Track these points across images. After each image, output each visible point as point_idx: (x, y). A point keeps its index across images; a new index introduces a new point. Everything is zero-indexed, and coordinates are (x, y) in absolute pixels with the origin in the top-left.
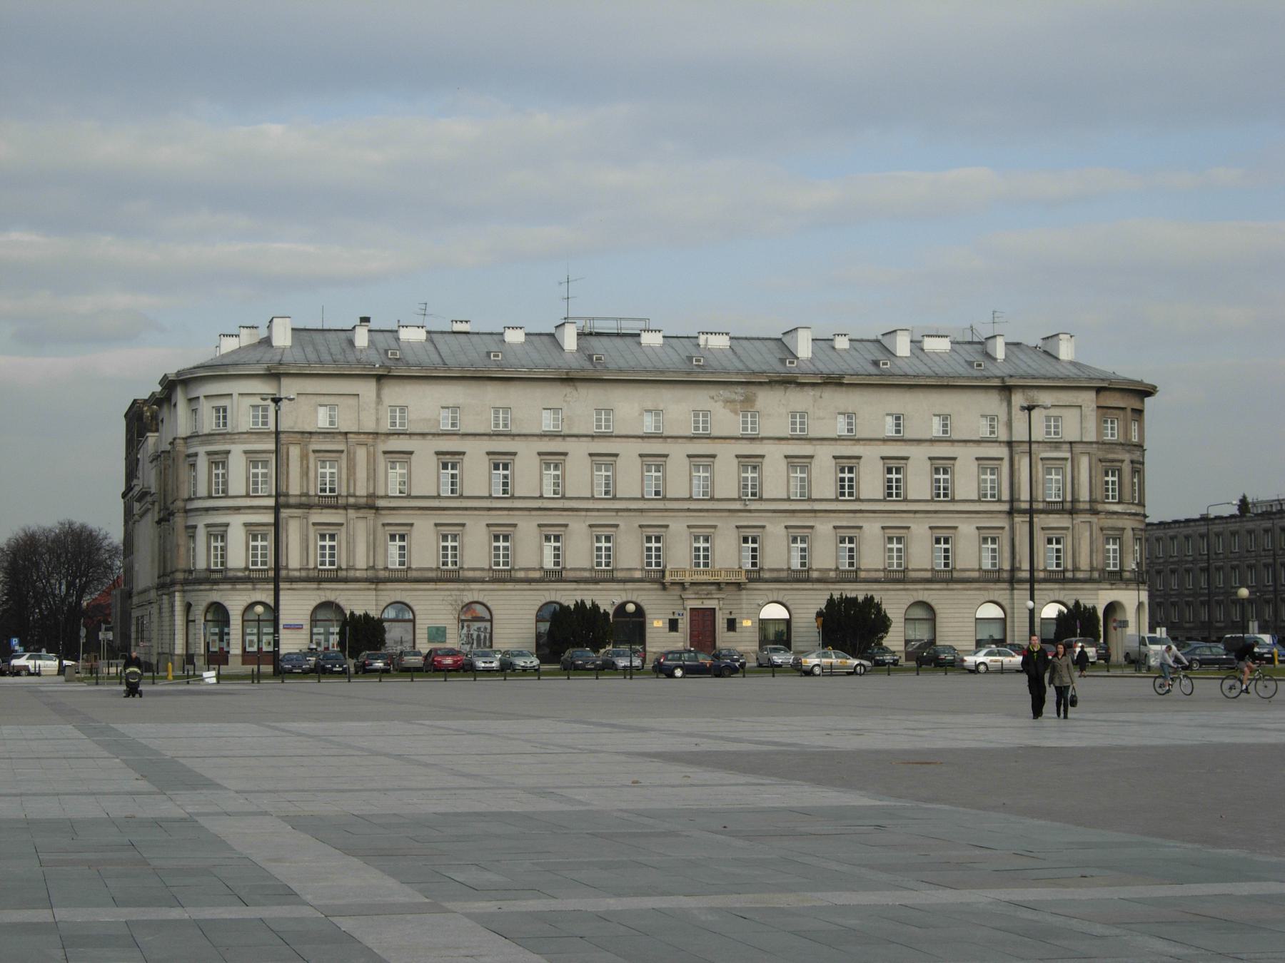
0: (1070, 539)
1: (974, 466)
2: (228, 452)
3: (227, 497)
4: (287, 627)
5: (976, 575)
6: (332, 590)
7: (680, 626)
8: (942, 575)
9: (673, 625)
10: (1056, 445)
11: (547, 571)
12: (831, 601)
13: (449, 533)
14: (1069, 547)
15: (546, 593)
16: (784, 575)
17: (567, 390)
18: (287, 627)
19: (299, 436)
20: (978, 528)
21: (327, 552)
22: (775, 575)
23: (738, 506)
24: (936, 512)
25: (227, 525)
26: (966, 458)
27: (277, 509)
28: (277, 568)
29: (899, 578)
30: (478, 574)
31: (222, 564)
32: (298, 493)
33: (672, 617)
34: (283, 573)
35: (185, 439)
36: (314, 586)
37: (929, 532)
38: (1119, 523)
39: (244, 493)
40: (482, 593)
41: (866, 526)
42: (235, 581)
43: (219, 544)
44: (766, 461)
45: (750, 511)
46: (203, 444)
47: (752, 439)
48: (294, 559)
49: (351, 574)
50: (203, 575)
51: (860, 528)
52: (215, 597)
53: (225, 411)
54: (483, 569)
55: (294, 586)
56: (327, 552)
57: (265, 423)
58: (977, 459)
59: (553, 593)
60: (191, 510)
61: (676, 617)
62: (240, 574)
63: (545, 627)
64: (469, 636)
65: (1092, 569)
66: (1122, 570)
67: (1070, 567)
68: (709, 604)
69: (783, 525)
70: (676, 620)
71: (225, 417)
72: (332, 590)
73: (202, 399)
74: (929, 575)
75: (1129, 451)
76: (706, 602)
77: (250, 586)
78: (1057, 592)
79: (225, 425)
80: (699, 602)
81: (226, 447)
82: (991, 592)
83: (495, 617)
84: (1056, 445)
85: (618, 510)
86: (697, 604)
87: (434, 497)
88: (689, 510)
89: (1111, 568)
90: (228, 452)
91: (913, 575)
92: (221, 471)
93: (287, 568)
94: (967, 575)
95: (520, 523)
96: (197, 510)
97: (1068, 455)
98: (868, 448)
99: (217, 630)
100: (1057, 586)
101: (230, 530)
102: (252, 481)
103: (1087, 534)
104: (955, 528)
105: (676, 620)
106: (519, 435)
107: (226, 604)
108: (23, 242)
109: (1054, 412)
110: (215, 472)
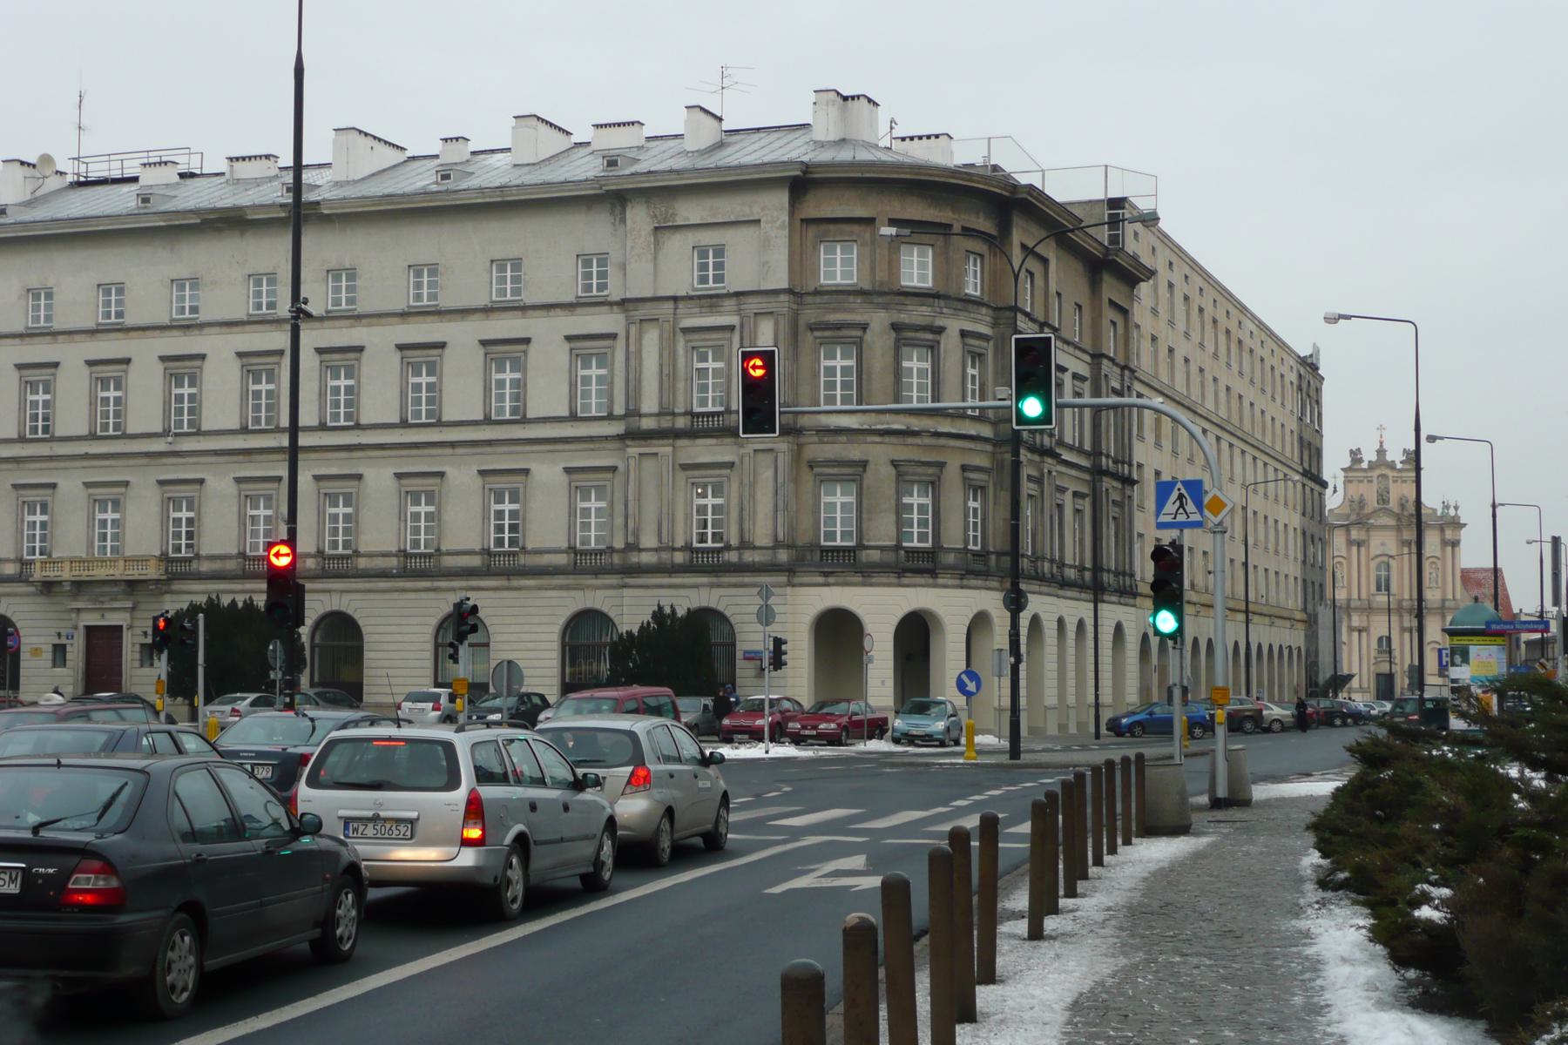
0: (735, 486)
1: (562, 353)
5: (562, 559)
7: (69, 656)
8: (502, 562)
9: (59, 652)
10: (711, 301)
11: (913, 552)
12: (658, 615)
13: (505, 482)
14: (734, 503)
16: (231, 565)
20: (568, 470)
22: (216, 566)
24: (489, 443)
26: (221, 350)
29: (416, 568)
30: (380, 563)
32: (655, 409)
33: (57, 641)
37: (479, 481)
38: (855, 452)
39: (397, 420)
40: (346, 598)
41: (369, 473)
44: (208, 365)
47: (186, 327)
49: (749, 557)
51: (359, 477)
55: (515, 582)
57: (271, 305)
58: (569, 338)
61: (63, 641)
65: (777, 545)
66: (861, 546)
67: (734, 542)
68: (112, 619)
69: (475, 469)
70: (64, 646)
74: (476, 561)
75: (886, 307)
76: (109, 615)
78: (705, 592)
80: (97, 616)
82: (589, 594)
84: (711, 301)
86: (94, 620)
88: (87, 456)
89: (915, 544)
91: (449, 562)
92: (186, 391)
94: (546, 560)
95: (533, 466)
97: (733, 320)
98: (375, 330)
100: (704, 580)
103: (769, 474)
104: (526, 472)
105: (64, 646)
106: (380, 316)
109: (709, 238)
110: (496, 376)
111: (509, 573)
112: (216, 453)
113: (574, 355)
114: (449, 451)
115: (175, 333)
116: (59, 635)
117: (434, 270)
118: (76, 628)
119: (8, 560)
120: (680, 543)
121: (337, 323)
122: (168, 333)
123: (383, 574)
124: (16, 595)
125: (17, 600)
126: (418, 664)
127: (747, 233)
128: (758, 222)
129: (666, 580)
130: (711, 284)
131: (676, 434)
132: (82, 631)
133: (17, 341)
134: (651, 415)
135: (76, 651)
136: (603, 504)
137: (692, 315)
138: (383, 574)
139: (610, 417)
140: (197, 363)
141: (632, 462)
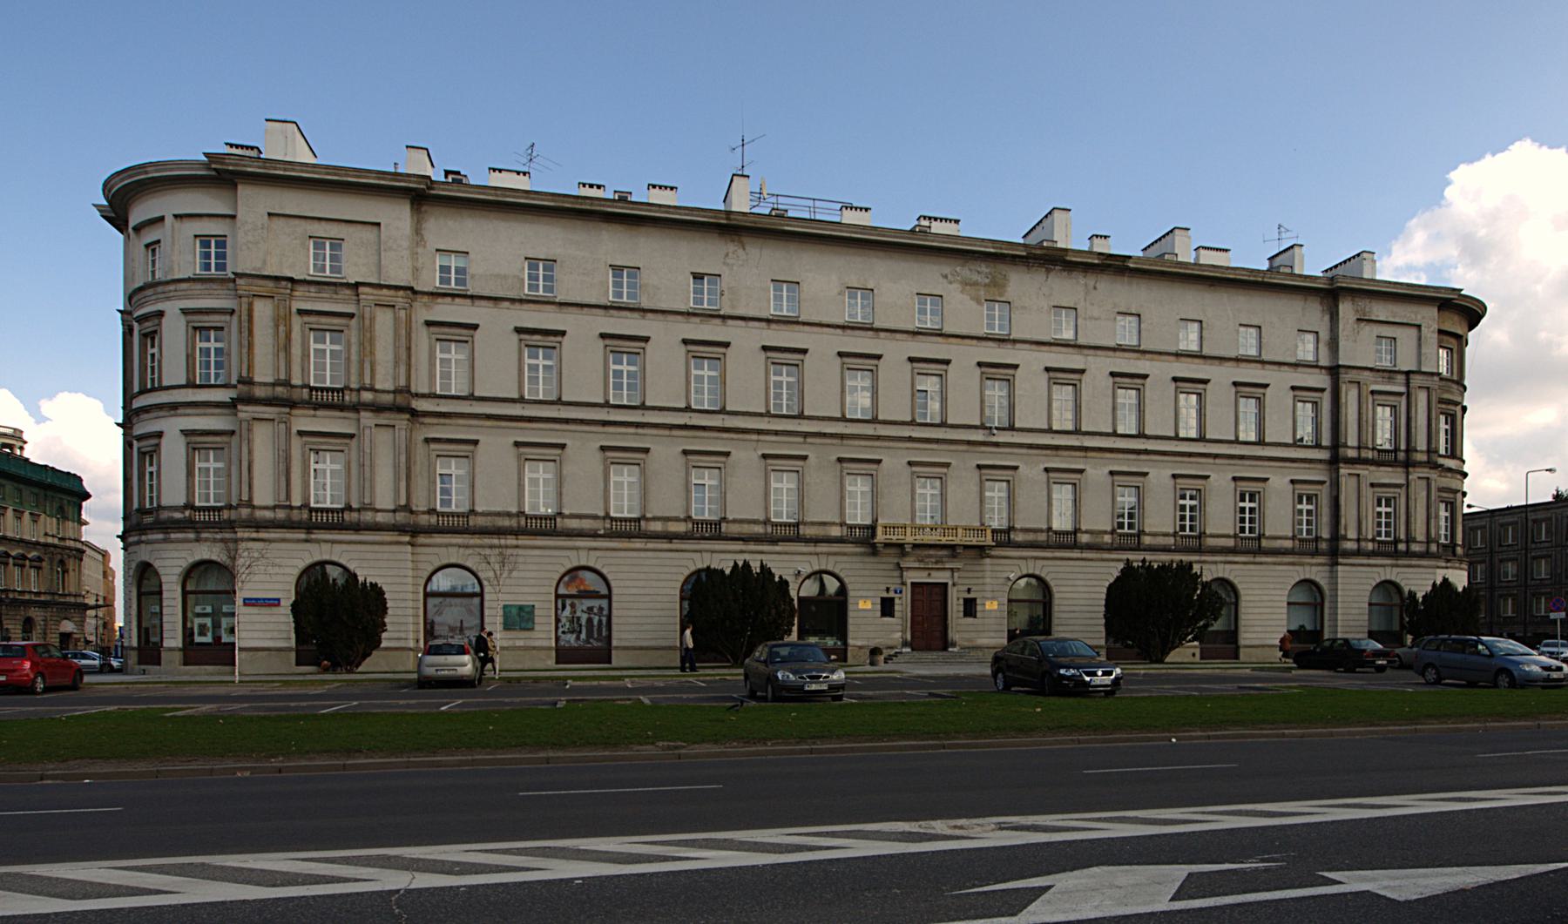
5: (1288, 544)
6: (333, 542)
9: (887, 607)
19: (270, 284)
22: (1031, 537)
24: (1242, 457)
27: (1335, 461)
28: (1336, 537)
30: (1161, 541)
33: (885, 595)
41: (1153, 473)
61: (892, 594)
70: (892, 600)
72: (333, 542)
74: (1230, 543)
81: (159, 307)
85: (806, 435)
86: (921, 577)
87: (513, 401)
88: (910, 439)
99: (209, 610)
100: (1389, 562)
101: (164, 441)
105: (892, 600)
111: (357, 528)
112: (1030, 446)
113: (844, 368)
114: (1211, 460)
115: (990, 344)
116: (888, 590)
117: (550, 262)
118: (903, 584)
119: (1106, 532)
120: (296, 502)
121: (1127, 355)
122: (984, 343)
123: (670, 537)
124: (845, 554)
125: (845, 558)
126: (625, 613)
127: (368, 234)
128: (378, 224)
129: (1365, 561)
130: (453, 285)
131: (1366, 462)
132: (908, 591)
133: (839, 331)
134: (265, 384)
135: (903, 605)
136: (220, 465)
137: (1376, 383)
138: (670, 537)
139: (1318, 446)
140: (1011, 372)
141: (245, 425)
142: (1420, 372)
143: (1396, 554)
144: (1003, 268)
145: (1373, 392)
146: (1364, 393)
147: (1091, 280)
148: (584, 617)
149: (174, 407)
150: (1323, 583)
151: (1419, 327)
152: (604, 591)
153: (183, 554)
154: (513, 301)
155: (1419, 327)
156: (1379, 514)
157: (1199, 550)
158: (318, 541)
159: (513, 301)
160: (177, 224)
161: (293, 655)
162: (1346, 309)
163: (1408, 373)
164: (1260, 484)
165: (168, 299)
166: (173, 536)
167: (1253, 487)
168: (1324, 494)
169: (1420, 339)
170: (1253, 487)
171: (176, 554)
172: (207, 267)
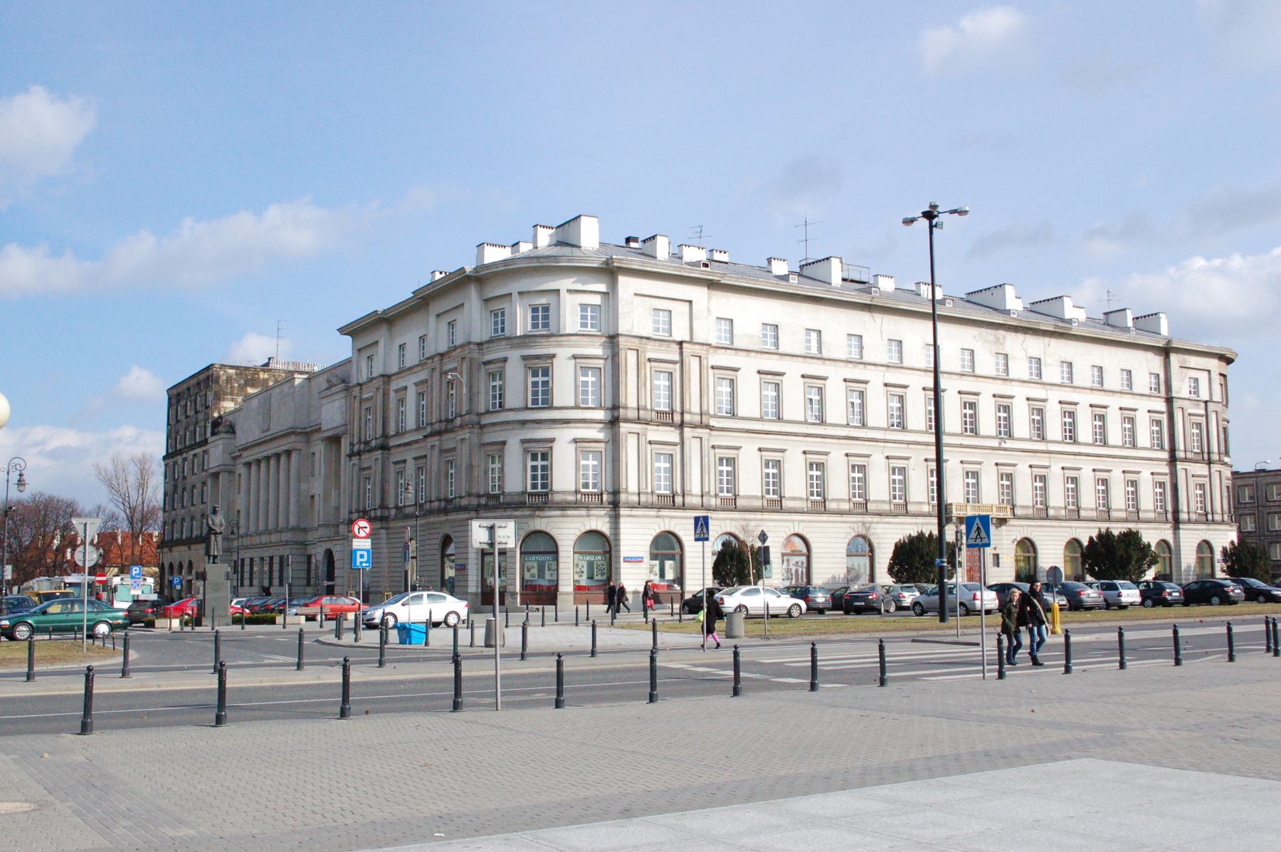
2: (505, 360)
3: (551, 408)
4: (628, 560)
15: (790, 524)
17: (865, 316)
18: (628, 560)
19: (637, 340)
21: (539, 473)
23: (995, 443)
25: (552, 440)
27: (614, 422)
28: (616, 493)
30: (797, 504)
31: (544, 486)
34: (623, 497)
35: (480, 344)
36: (653, 512)
40: (674, 521)
42: (564, 506)
43: (498, 383)
45: (1005, 449)
46: (513, 347)
48: (630, 483)
50: (516, 499)
52: (539, 524)
53: (503, 314)
54: (801, 499)
56: (539, 473)
59: (667, 520)
60: (485, 426)
62: (571, 498)
63: (1195, 587)
64: (788, 571)
71: (503, 323)
73: (515, 296)
77: (583, 512)
79: (503, 329)
81: (551, 351)
83: (814, 550)
85: (909, 443)
87: (757, 420)
88: (962, 446)
90: (505, 360)
92: (498, 383)
93: (627, 492)
96: (494, 424)
101: (556, 446)
102: (580, 389)
107: (553, 533)
108: (21, 268)
112: (1023, 451)
142: (691, 342)
143: (674, 506)
144: (1001, 332)
145: (649, 360)
146: (642, 360)
147: (1047, 340)
148: (794, 569)
149: (567, 422)
150: (1171, 541)
151: (690, 302)
152: (805, 551)
153: (577, 525)
154: (757, 352)
155: (690, 302)
156: (721, 472)
157: (1139, 520)
158: (663, 517)
159: (757, 352)
160: (568, 295)
161: (572, 597)
162: (1174, 358)
163: (681, 343)
164: (781, 454)
165: (560, 346)
166: (569, 512)
167: (777, 456)
168: (1167, 479)
169: (1210, 379)
170: (777, 456)
171: (571, 525)
172: (584, 325)
